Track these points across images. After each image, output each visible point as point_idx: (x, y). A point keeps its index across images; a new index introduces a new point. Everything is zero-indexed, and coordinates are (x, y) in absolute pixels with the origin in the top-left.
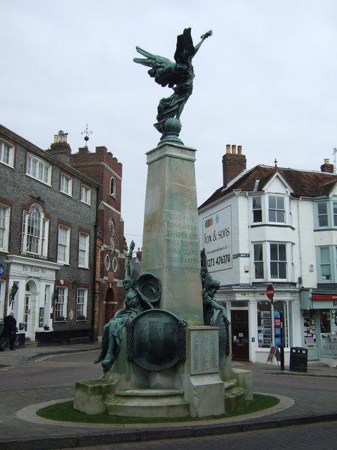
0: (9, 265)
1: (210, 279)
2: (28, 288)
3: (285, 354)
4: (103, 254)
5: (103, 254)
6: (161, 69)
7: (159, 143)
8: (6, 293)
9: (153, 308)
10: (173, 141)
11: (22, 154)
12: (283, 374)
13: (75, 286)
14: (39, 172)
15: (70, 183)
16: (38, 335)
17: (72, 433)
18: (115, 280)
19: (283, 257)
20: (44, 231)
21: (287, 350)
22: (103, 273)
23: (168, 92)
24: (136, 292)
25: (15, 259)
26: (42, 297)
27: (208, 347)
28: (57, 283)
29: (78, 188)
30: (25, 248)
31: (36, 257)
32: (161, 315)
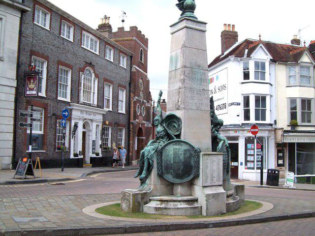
0: (71, 110)
1: (216, 118)
2: (84, 127)
3: (264, 174)
4: (135, 103)
5: (135, 103)
7: (180, 18)
8: (70, 130)
9: (176, 139)
10: (190, 16)
11: (79, 31)
12: (262, 187)
13: (116, 125)
14: (89, 44)
15: (112, 52)
16: (92, 159)
17: (121, 225)
18: (143, 122)
19: (264, 105)
20: (94, 87)
21: (265, 171)
22: (135, 117)
24: (164, 127)
25: (75, 106)
26: (94, 135)
27: (215, 168)
28: (104, 123)
29: (118, 56)
30: (82, 100)
31: (90, 105)
32: (182, 144)
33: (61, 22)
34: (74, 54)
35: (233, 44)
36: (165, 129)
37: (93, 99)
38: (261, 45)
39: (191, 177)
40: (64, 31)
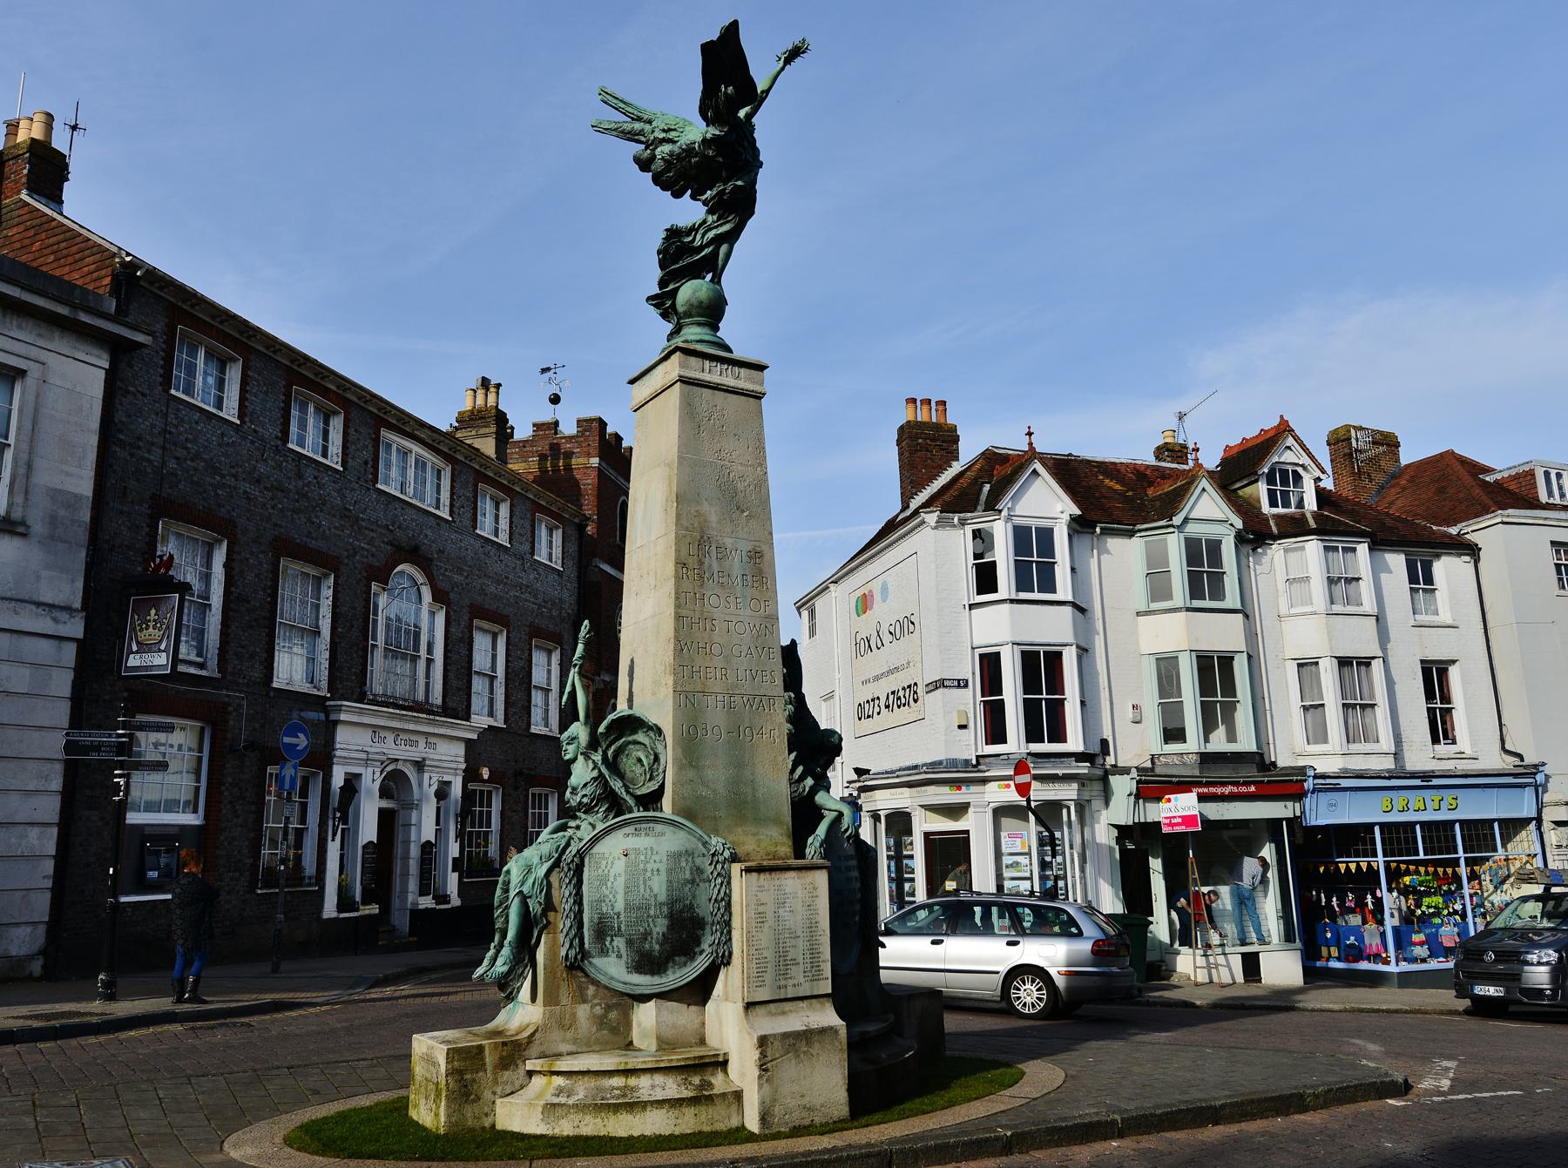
6: (666, 148)
23: (689, 211)
25: (348, 712)
28: (470, 775)
32: (659, 827)
33: (288, 396)
34: (345, 514)
35: (941, 469)
36: (601, 774)
37: (427, 685)
38: (1038, 466)
39: (700, 964)
40: (388, 465)
